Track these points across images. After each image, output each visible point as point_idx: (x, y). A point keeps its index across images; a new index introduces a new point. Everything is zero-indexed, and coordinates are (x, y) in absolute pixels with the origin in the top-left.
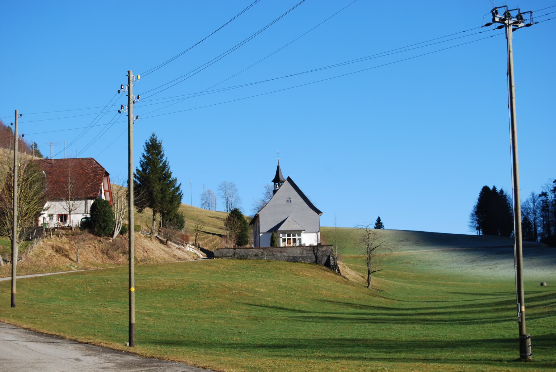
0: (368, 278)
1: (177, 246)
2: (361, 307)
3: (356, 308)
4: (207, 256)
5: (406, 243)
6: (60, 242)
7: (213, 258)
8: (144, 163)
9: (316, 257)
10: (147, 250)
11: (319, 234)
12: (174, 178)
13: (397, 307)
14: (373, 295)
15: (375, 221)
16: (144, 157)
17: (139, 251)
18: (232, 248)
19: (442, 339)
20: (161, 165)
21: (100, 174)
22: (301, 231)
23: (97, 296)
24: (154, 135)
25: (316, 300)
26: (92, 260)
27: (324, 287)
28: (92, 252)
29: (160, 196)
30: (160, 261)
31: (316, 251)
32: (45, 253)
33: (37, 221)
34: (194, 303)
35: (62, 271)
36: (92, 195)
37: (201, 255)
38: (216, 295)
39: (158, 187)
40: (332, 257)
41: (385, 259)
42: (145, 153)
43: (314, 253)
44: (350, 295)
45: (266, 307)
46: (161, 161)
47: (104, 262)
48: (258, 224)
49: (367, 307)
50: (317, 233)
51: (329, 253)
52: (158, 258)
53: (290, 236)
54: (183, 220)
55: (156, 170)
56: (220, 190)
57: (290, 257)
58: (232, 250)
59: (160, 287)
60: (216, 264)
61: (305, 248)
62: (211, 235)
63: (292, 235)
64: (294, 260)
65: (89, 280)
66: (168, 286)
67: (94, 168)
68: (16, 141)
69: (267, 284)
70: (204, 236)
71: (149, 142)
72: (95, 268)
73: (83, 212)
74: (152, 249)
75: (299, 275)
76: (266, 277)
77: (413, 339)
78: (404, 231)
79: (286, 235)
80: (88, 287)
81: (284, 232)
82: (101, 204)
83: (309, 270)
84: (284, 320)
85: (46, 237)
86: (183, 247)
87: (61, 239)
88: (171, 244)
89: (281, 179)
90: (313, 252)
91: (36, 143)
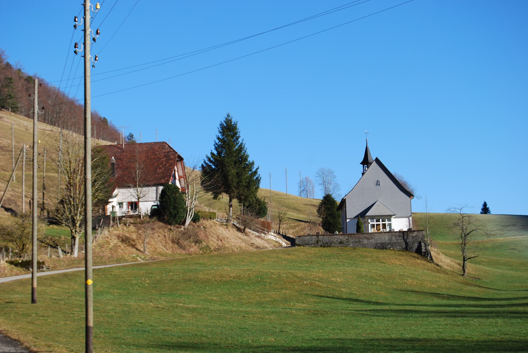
0: (464, 265)
1: (257, 234)
2: (450, 297)
3: (443, 299)
4: (291, 245)
5: (512, 228)
6: (127, 232)
7: (295, 247)
8: (218, 146)
9: (407, 244)
10: (221, 239)
11: (411, 218)
12: (251, 161)
13: (490, 297)
14: (467, 284)
15: (481, 207)
16: (218, 140)
17: (213, 239)
18: (314, 235)
19: (523, 338)
20: (236, 147)
21: (173, 159)
22: (391, 216)
23: (153, 289)
24: (228, 116)
25: (399, 290)
26: (161, 250)
27: (410, 275)
28: (162, 242)
29: (236, 180)
30: (236, 250)
31: (406, 237)
32: (110, 243)
33: (104, 210)
34: (256, 295)
35: (127, 263)
36: (163, 181)
37: (284, 243)
38: (285, 286)
39: (233, 171)
40: (424, 242)
41: (488, 245)
42: (220, 135)
43: (404, 239)
44: (439, 284)
45: (338, 299)
46: (236, 143)
47: (174, 252)
48: (345, 210)
49: (456, 297)
50: (408, 217)
51: (420, 239)
52: (234, 246)
53: (380, 222)
54: (265, 206)
55: (231, 153)
56: (317, 177)
57: (377, 243)
58: (314, 237)
59: (224, 279)
60: (296, 253)
61: (394, 234)
62: (303, 223)
63: (381, 220)
64: (382, 247)
65: (151, 271)
66: (233, 276)
67: (166, 152)
68: (35, 114)
69: (346, 273)
70: (296, 224)
71: (224, 123)
72: (163, 258)
73: (155, 199)
74: (228, 238)
75: (386, 264)
76: (349, 266)
77: (486, 338)
78: (510, 216)
79: (375, 220)
80: (147, 279)
81: (372, 218)
82: (171, 190)
83: (398, 257)
84: (347, 315)
85: (112, 226)
86: (264, 235)
87: (128, 229)
88: (249, 232)
89: (370, 161)
90: (402, 238)
91: (132, 133)
